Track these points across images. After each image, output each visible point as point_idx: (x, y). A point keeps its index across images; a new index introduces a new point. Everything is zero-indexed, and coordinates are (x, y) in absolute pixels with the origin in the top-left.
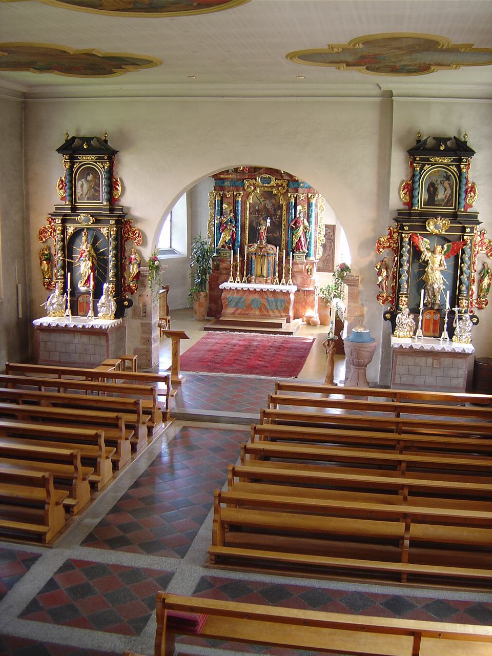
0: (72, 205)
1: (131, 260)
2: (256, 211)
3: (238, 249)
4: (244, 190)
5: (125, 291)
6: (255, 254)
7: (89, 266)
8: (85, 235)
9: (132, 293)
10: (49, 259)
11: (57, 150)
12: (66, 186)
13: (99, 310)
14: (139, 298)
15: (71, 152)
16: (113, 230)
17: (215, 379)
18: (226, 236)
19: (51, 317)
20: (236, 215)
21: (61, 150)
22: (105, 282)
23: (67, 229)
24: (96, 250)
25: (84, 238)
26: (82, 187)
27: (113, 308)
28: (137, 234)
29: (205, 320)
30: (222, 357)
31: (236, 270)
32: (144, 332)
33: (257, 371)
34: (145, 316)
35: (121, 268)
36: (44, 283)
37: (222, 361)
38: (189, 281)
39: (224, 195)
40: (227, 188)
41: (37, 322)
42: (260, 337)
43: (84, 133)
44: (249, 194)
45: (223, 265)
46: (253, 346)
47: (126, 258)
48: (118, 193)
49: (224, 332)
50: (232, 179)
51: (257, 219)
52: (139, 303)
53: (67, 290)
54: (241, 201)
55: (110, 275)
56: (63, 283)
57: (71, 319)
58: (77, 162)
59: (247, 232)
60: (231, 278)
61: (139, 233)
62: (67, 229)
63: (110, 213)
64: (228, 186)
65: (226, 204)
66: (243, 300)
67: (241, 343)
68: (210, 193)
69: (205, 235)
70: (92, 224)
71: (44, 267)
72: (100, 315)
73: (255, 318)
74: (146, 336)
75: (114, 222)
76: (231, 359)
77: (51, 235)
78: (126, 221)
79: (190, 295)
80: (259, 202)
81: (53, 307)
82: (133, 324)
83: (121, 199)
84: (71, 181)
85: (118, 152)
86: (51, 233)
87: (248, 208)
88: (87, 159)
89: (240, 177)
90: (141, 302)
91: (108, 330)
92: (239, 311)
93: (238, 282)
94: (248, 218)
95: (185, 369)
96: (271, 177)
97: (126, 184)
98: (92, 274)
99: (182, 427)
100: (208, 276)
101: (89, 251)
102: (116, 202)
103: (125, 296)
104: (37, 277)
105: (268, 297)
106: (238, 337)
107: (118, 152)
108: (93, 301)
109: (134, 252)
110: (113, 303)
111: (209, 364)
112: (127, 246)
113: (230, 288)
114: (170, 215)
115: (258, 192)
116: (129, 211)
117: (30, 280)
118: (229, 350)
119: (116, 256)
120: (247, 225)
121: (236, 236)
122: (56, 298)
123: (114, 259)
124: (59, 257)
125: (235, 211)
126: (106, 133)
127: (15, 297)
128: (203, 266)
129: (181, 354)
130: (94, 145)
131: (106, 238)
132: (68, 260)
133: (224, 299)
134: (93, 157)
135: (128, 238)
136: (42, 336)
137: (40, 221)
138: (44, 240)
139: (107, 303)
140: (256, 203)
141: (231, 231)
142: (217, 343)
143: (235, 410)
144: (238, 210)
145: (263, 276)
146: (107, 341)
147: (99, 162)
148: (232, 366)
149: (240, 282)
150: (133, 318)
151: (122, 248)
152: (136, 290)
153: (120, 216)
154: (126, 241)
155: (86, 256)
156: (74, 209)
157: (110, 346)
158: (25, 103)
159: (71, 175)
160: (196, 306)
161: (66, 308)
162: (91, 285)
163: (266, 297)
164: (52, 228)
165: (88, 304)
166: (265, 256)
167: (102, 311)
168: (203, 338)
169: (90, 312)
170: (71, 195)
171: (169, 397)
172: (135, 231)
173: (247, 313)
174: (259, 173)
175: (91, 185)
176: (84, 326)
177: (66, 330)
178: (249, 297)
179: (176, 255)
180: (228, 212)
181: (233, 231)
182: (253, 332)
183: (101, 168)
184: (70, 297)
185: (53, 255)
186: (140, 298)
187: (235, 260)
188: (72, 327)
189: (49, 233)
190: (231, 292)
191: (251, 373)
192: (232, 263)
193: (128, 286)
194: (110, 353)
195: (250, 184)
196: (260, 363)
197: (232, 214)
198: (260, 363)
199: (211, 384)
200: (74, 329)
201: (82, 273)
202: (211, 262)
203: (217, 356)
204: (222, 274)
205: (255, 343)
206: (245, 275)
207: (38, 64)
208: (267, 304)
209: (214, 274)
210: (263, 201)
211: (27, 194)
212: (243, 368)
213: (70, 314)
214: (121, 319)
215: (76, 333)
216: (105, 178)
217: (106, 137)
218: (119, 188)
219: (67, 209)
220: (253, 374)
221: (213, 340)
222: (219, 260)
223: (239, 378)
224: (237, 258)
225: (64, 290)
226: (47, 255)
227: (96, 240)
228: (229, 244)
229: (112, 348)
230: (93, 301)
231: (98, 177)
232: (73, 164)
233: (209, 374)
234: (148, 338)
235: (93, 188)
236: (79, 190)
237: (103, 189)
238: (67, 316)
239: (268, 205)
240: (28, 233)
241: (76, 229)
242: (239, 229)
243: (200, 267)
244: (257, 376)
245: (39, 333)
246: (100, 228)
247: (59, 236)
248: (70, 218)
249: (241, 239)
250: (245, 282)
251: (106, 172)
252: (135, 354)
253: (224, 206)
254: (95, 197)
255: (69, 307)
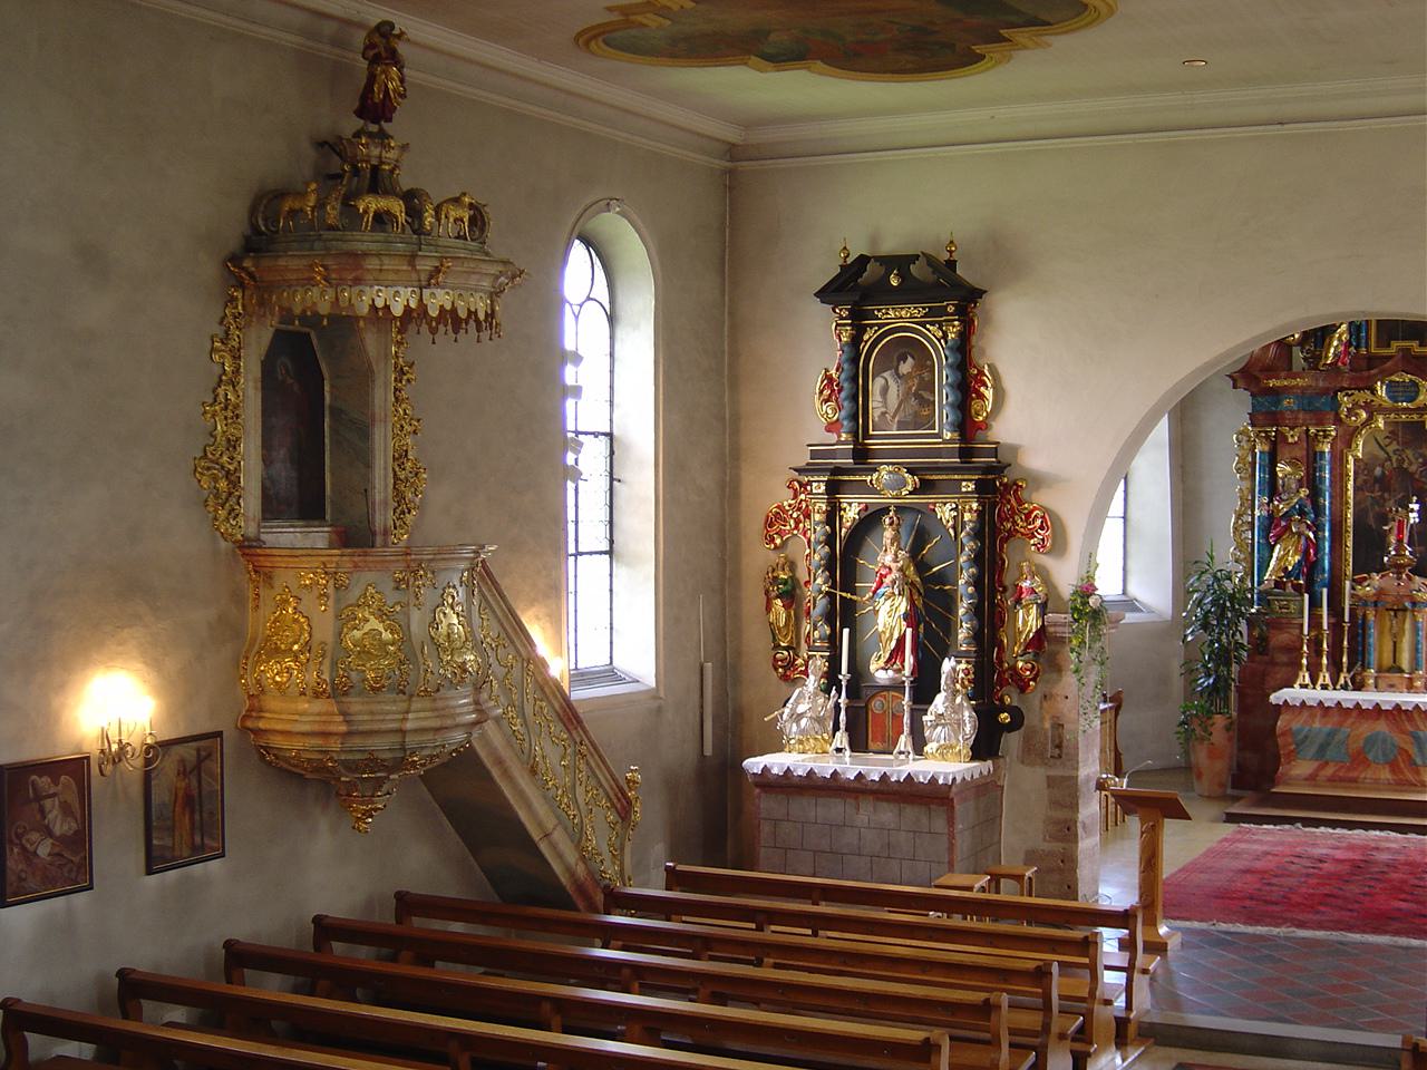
0: (856, 442)
1: (1021, 593)
2: (1378, 480)
3: (1325, 591)
4: (1338, 421)
5: (1002, 683)
6: (1376, 606)
7: (903, 609)
8: (891, 524)
9: (1023, 687)
10: (791, 595)
11: (816, 295)
12: (840, 391)
13: (927, 734)
14: (1041, 703)
15: (857, 298)
16: (971, 510)
17: (1269, 943)
18: (1285, 555)
19: (794, 754)
20: (1315, 494)
21: (828, 294)
22: (944, 654)
23: (841, 509)
24: (921, 566)
25: (888, 534)
26: (885, 395)
27: (968, 728)
28: (1038, 522)
29: (1223, 798)
30: (1287, 890)
31: (1319, 653)
32: (1055, 803)
33: (1396, 925)
34: (1060, 756)
35: (990, 618)
36: (776, 660)
37: (1285, 897)
38: (1177, 683)
39: (1281, 438)
40: (1288, 415)
41: (754, 764)
42: (1396, 841)
43: (889, 247)
44: (1355, 431)
45: (1281, 638)
46: (1376, 863)
47: (1005, 589)
48: (983, 408)
49: (1287, 827)
50: (1303, 389)
51: (1378, 504)
52: (1042, 719)
53: (840, 677)
54: (1331, 452)
55: (960, 637)
56: (829, 659)
57: (847, 759)
58: (871, 326)
59: (1350, 544)
60: (1305, 677)
61: (1043, 517)
62: (841, 509)
63: (962, 463)
64: (1292, 411)
65: (1288, 464)
66: (1340, 737)
67: (1339, 854)
68: (1240, 433)
69: (1226, 553)
70: (910, 493)
71: (778, 614)
72: (930, 748)
73: (1379, 790)
74: (1060, 814)
75: (972, 486)
76: (1313, 895)
77: (796, 527)
78: (1005, 485)
79: (1183, 723)
80: (1382, 455)
81: (798, 726)
82: (1024, 782)
83: (993, 423)
84: (854, 379)
85: (985, 292)
86: (797, 522)
87: (1352, 474)
88: (898, 317)
89: (1327, 385)
90: (1047, 717)
91: (954, 789)
92: (1329, 771)
93: (1324, 687)
94: (1351, 501)
95: (1177, 914)
96: (1418, 380)
97: (1009, 382)
98: (909, 631)
99: (1174, 1064)
100: (1235, 668)
101: (901, 570)
102: (980, 431)
103: (1002, 696)
104: (756, 644)
105: (1418, 729)
106: (1328, 842)
107: (985, 292)
108: (912, 709)
109: (1030, 571)
110: (968, 715)
111: (1247, 903)
112: (1010, 554)
113: (1303, 703)
114: (1123, 481)
115: (1381, 425)
116: (1016, 457)
117: (738, 654)
118: (1304, 871)
119: (977, 582)
120: (1350, 522)
121: (1315, 555)
122: (807, 701)
123: (971, 589)
124: (817, 586)
125: (1313, 482)
126: (952, 242)
127: (696, 696)
128: (1219, 641)
129: (1164, 876)
130: (922, 279)
131: (951, 531)
132: (844, 594)
133: (1283, 734)
134: (916, 311)
135: (1011, 534)
136: (767, 805)
137: (770, 490)
138: (778, 541)
139: (951, 716)
140: (1375, 457)
141: (1303, 541)
142: (1267, 853)
143: (1336, 1024)
144: (1322, 479)
145: (1401, 671)
146: (951, 822)
147: (932, 324)
148: (1317, 913)
149: (1331, 687)
150: (1023, 762)
151: (995, 562)
152: (1034, 679)
153: (988, 469)
154: (1006, 540)
155: (894, 582)
156: (862, 454)
157: (958, 836)
158: (731, 172)
159: (854, 360)
160: (1201, 756)
161: (836, 728)
162: (907, 664)
163: (1410, 728)
164: (799, 509)
165: (898, 718)
166: (1405, 610)
167: (936, 737)
168: (1226, 840)
169: (903, 738)
170: (854, 417)
171: (1136, 976)
172: (1032, 512)
173: (1355, 774)
174: (1381, 372)
175: (910, 388)
176: (884, 777)
177: (833, 787)
178: (1361, 730)
179: (1137, 615)
180: (1294, 486)
181: (1308, 538)
182: (1375, 829)
183: (938, 340)
184: (847, 697)
185: (802, 583)
186: (1045, 704)
187: (1315, 622)
188: (852, 778)
189: (792, 522)
190: (1306, 714)
191: (1376, 931)
192: (1306, 632)
193: (1009, 668)
194: (958, 856)
195: (1356, 405)
196: (1403, 905)
197: (1304, 492)
198: (1403, 905)
199: (1258, 954)
200: (856, 785)
201: (880, 630)
202: (1243, 626)
203: (1269, 884)
204: (1277, 664)
205: (1384, 857)
206: (1345, 666)
207: (773, 37)
208: (1413, 751)
209: (1254, 665)
210: (1394, 452)
211: (736, 418)
212: (1351, 917)
213: (845, 744)
214: (990, 762)
215: (861, 797)
216: (950, 366)
217: (951, 252)
218: (989, 394)
219: (842, 453)
220: (1385, 932)
221: (1255, 847)
222: (1269, 623)
223: (1341, 943)
224: (1321, 616)
225: (831, 680)
226: (785, 582)
227: (920, 538)
228: (1297, 578)
229: (963, 843)
230: (912, 711)
231: (929, 363)
232: (859, 331)
233: (1250, 929)
234: (1066, 821)
235: (917, 396)
236: (875, 403)
237: (943, 397)
238: (839, 750)
239: (1411, 464)
240: (736, 525)
241: (866, 508)
242: (1327, 534)
243: (1212, 642)
244: (1396, 939)
245: (759, 797)
246: (934, 504)
247: (818, 529)
248: (852, 478)
249: (1330, 563)
250: (1345, 687)
251: (950, 349)
252: (1028, 862)
253: (1282, 469)
254: (922, 420)
255: (842, 726)
